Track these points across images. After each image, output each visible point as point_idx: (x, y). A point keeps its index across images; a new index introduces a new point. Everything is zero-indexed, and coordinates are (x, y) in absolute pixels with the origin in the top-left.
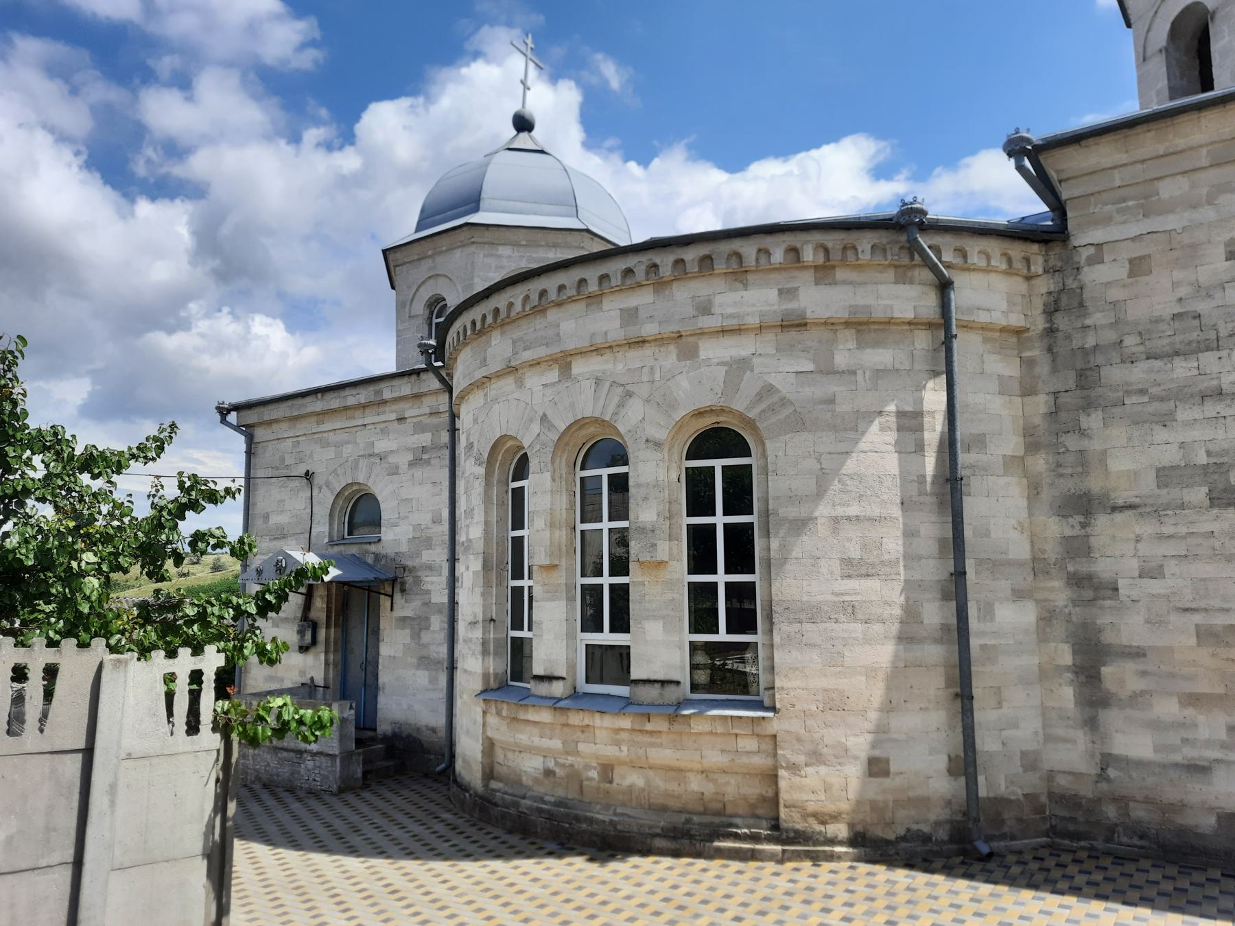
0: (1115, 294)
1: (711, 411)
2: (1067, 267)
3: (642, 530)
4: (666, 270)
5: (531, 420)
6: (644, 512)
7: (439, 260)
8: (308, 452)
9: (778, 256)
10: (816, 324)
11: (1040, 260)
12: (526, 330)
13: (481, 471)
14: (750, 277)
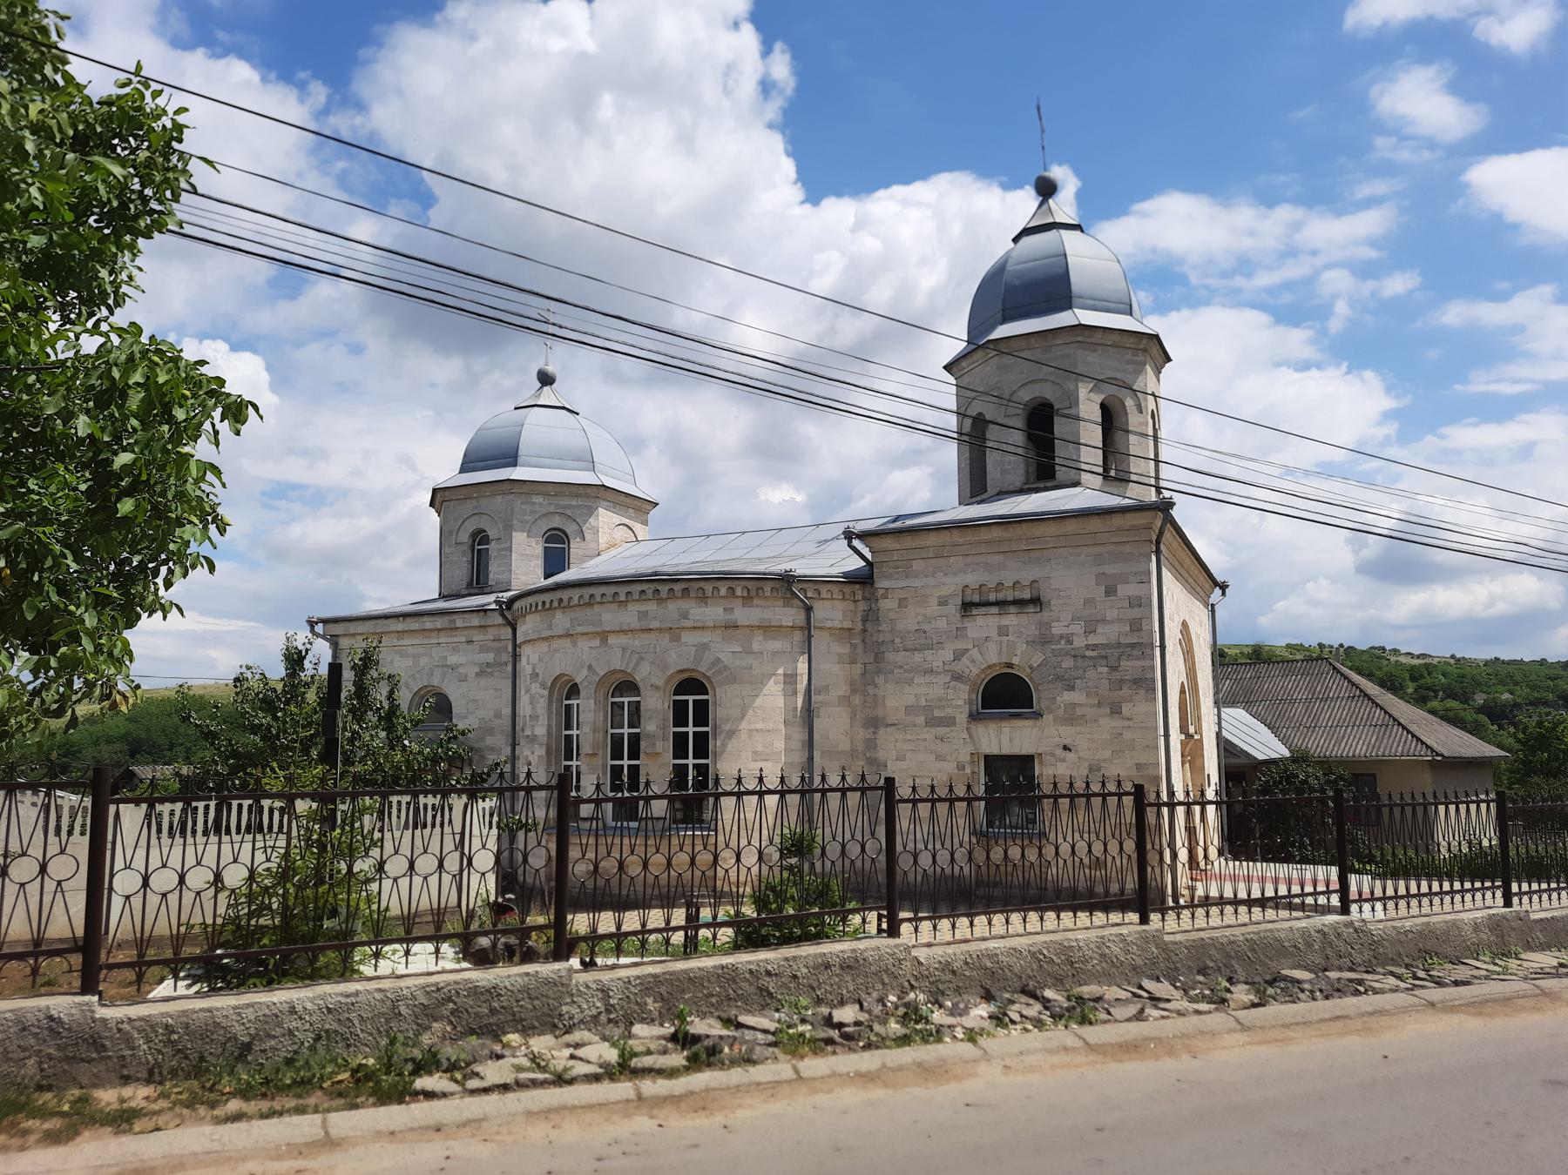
0: (892, 615)
1: (687, 670)
2: (872, 599)
3: (648, 736)
4: (664, 594)
5: (582, 667)
6: (649, 726)
7: (483, 501)
8: (389, 660)
9: (723, 592)
10: (743, 626)
11: (860, 592)
12: (580, 614)
13: (546, 693)
14: (709, 600)
